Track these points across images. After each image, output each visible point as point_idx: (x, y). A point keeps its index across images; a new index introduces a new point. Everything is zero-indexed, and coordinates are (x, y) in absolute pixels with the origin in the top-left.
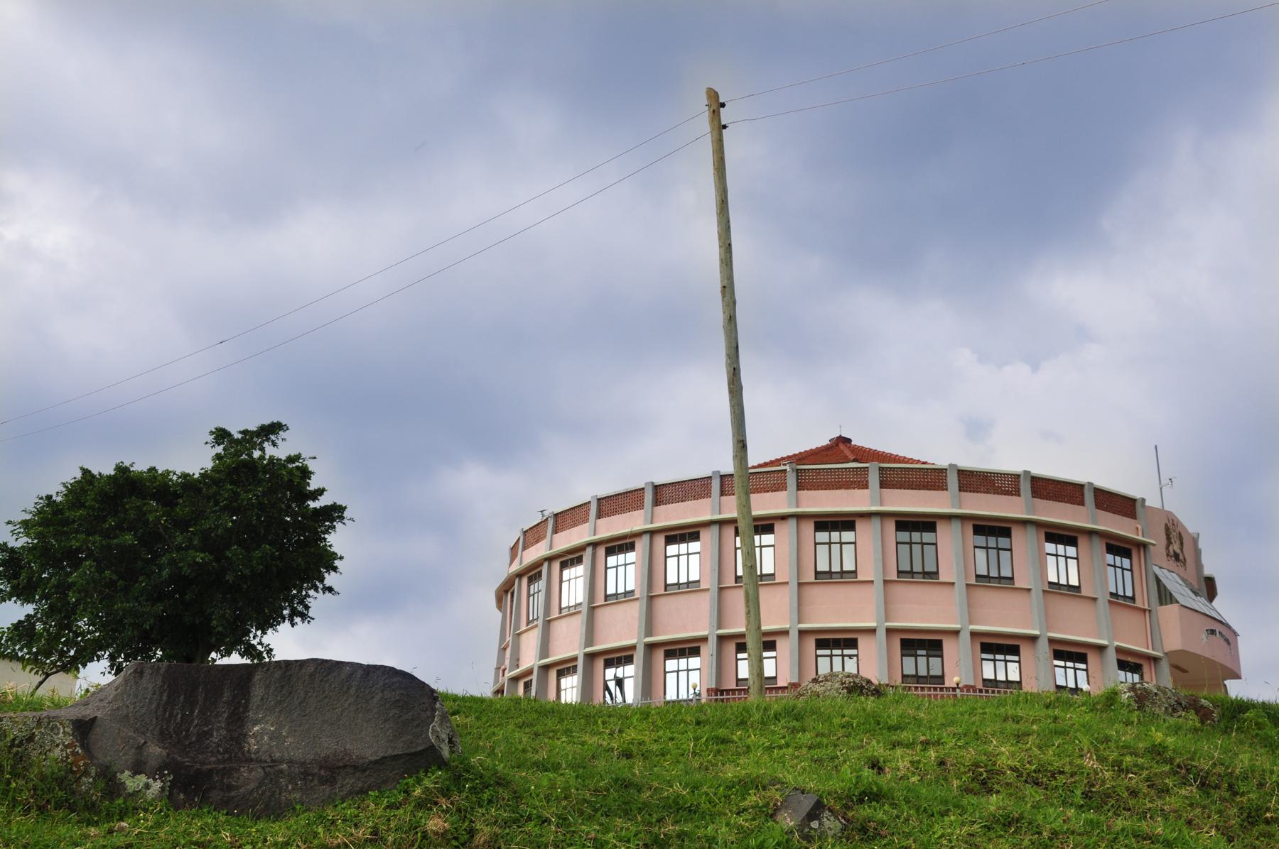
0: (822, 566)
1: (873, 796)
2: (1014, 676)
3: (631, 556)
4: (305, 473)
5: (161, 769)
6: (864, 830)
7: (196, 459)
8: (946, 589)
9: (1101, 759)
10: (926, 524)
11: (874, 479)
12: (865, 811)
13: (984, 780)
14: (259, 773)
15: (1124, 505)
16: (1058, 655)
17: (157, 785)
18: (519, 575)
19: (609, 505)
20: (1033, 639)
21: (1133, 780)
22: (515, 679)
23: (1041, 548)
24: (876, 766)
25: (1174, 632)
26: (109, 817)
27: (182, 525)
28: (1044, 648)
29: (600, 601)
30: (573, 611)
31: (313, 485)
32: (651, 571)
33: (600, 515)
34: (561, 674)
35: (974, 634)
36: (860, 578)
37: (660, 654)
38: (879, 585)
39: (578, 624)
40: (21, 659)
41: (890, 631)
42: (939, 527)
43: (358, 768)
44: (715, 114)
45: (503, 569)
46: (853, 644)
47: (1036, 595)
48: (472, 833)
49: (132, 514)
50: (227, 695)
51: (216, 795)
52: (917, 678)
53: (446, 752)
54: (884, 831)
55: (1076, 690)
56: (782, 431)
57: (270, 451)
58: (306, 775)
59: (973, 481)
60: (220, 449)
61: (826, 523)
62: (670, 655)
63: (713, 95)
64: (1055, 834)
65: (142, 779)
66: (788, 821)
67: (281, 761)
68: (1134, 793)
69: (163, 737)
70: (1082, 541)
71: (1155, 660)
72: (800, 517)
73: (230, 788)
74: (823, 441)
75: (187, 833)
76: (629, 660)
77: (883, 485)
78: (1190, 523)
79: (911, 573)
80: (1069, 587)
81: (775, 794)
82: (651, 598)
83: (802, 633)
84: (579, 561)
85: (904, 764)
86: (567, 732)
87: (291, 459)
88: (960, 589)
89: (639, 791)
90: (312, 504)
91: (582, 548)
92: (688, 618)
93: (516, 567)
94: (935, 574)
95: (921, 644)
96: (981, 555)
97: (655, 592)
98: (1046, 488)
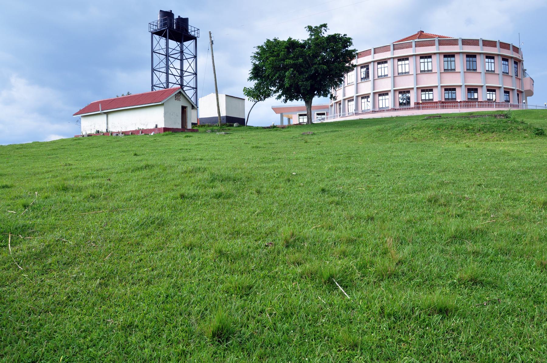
8: (478, 75)
11: (414, 44)
15: (516, 50)
16: (488, 90)
22: (337, 103)
23: (484, 60)
33: (375, 53)
35: (466, 86)
36: (456, 71)
39: (353, 88)
41: (441, 86)
42: (456, 56)
46: (431, 90)
61: (423, 57)
62: (380, 95)
63: (210, 32)
88: (462, 73)
95: (472, 89)
98: (487, 43)
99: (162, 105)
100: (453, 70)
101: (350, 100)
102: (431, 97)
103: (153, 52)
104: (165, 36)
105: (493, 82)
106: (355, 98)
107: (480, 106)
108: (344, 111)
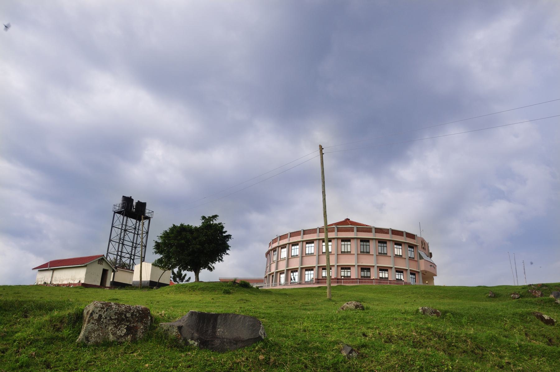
0: (343, 250)
1: (364, 346)
2: (387, 276)
3: (298, 247)
4: (223, 227)
5: (197, 339)
6: (362, 356)
7: (197, 223)
9: (417, 332)
10: (367, 240)
11: (355, 230)
12: (363, 350)
13: (389, 340)
14: (219, 342)
15: (412, 236)
16: (397, 271)
17: (196, 343)
18: (271, 250)
19: (293, 234)
20: (391, 268)
21: (423, 337)
22: (270, 275)
24: (364, 335)
25: (423, 266)
26: (186, 351)
27: (195, 239)
28: (394, 270)
29: (290, 257)
30: (284, 259)
31: (224, 230)
32: (302, 250)
33: (290, 237)
34: (281, 274)
35: (378, 267)
37: (304, 270)
38: (356, 255)
40: (159, 267)
41: (358, 266)
43: (242, 341)
44: (321, 151)
45: (267, 248)
46: (349, 269)
47: (392, 258)
48: (269, 358)
49: (184, 236)
50: (212, 322)
51: (210, 346)
52: (364, 277)
53: (263, 337)
54: (367, 356)
55: (401, 280)
56: (334, 218)
57: (215, 222)
58: (230, 342)
59: (379, 230)
60: (203, 221)
62: (306, 270)
63: (321, 146)
64: (406, 355)
65: (193, 341)
66: (344, 354)
67: (224, 338)
68: (424, 341)
69: (197, 331)
70: (403, 245)
71: (419, 272)
72: (338, 238)
73: (213, 345)
74: (343, 219)
75: (203, 357)
76: (297, 271)
77: (357, 231)
78: (427, 240)
79: (364, 252)
80: (400, 255)
81: (341, 346)
82: (302, 257)
83: (338, 266)
84: (285, 247)
85: (370, 334)
86: (290, 324)
87: (219, 224)
88: (375, 256)
89: (308, 343)
90: (224, 235)
91: (286, 244)
92: (311, 262)
93: (270, 248)
94: (369, 252)
95: (365, 269)
96: (380, 248)
97: (303, 255)
98: (395, 232)
99: (86, 266)
100: (385, 254)
101: (282, 272)
102: (349, 275)
103: (112, 227)
104: (122, 215)
105: (401, 265)
106: (285, 271)
107: (353, 282)
108: (276, 281)
